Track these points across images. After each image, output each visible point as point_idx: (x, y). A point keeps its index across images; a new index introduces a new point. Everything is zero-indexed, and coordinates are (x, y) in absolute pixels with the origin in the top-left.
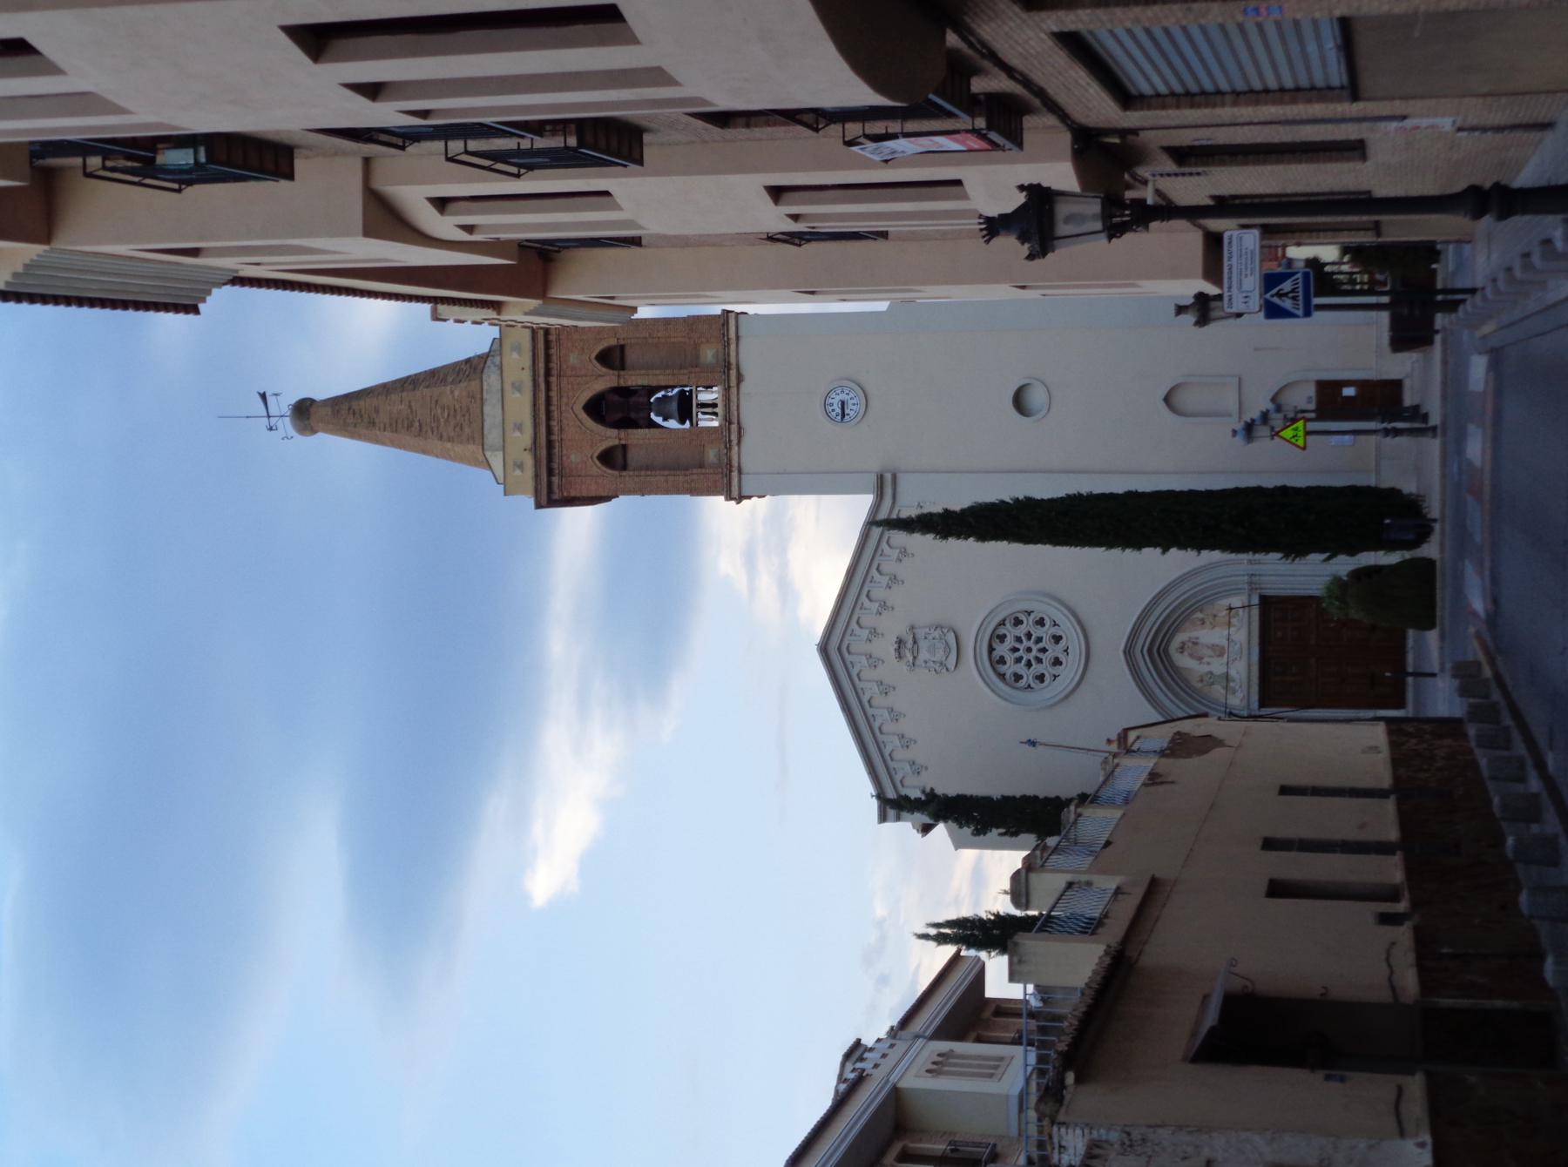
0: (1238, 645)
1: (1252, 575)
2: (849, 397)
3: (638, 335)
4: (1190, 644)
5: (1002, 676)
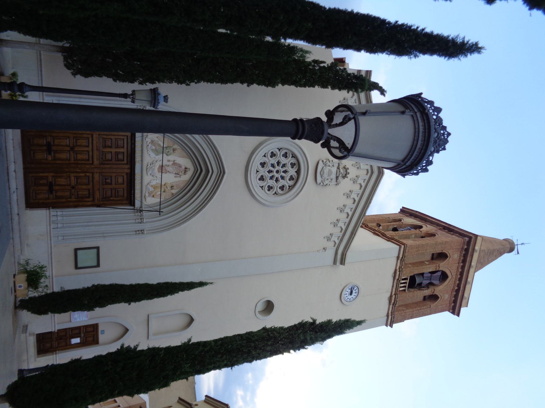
0: (149, 174)
1: (141, 223)
2: (348, 297)
3: (423, 310)
4: (181, 174)
5: (294, 156)
